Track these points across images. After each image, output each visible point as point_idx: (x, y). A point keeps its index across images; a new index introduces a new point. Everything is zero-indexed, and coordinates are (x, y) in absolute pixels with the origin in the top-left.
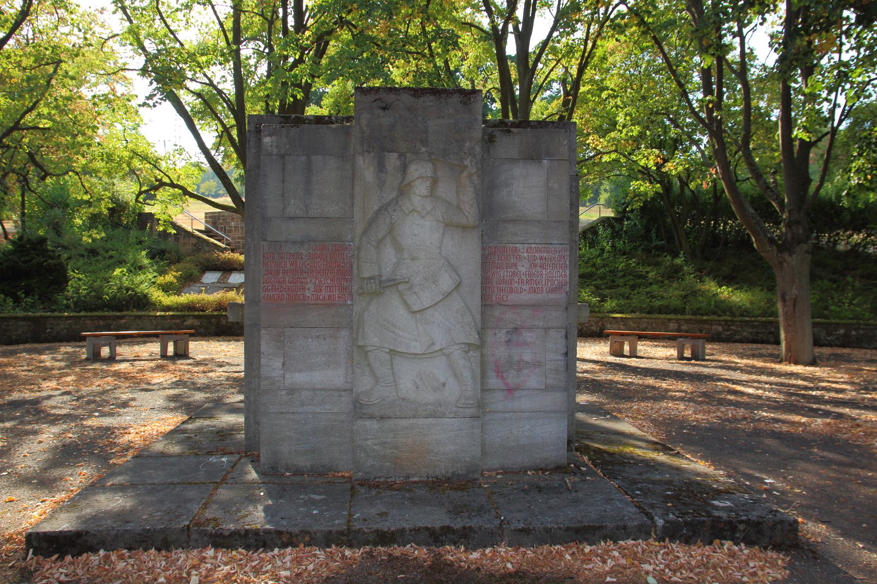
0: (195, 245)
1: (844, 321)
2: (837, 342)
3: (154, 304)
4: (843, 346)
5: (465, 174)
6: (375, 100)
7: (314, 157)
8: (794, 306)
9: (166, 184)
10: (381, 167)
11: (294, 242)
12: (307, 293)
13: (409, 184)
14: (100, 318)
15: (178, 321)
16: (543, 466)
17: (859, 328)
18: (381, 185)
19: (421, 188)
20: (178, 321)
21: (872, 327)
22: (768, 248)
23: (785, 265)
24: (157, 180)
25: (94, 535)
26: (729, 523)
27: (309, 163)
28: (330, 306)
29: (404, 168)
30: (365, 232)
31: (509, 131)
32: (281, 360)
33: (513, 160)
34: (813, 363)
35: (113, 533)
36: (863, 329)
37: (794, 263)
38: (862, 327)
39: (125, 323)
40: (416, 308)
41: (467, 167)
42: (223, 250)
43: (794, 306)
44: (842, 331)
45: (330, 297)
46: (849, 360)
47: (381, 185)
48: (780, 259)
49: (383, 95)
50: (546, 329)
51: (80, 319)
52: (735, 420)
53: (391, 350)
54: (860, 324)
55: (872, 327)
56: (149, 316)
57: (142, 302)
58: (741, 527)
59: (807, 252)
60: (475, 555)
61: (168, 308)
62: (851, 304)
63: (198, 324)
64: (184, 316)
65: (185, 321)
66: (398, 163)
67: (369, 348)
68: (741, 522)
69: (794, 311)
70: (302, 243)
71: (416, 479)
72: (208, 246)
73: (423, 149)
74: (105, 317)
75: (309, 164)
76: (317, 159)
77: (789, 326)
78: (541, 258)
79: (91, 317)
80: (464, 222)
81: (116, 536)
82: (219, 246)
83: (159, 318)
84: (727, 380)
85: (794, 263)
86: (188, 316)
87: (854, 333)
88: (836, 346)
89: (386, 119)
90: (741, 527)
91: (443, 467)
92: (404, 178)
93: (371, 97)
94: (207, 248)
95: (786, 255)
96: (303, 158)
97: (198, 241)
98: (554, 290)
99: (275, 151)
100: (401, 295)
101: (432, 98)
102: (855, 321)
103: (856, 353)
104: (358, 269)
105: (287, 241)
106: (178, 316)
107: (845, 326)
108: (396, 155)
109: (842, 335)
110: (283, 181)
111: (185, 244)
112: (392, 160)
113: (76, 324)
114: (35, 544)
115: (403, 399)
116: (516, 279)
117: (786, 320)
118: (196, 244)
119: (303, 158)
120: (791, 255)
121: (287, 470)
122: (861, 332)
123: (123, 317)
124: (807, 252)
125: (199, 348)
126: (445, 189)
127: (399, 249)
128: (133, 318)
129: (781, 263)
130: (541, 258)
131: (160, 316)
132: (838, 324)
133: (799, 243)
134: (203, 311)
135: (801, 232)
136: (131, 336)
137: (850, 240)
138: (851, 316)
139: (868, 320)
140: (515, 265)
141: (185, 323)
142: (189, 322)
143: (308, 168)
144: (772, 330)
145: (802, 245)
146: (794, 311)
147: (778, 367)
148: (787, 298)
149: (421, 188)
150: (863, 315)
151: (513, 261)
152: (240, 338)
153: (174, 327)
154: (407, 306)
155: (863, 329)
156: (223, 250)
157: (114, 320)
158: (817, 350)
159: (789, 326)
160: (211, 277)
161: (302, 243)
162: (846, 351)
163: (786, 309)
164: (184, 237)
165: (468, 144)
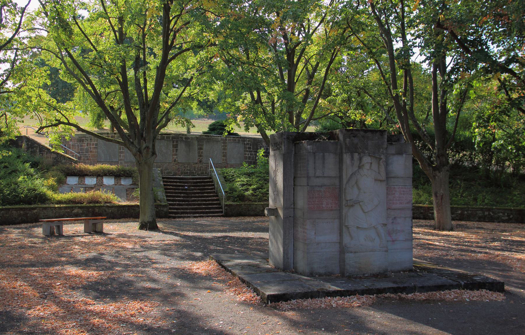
0: (55, 158)
1: (459, 206)
2: (457, 218)
3: (50, 200)
4: (461, 220)
5: (381, 161)
6: (351, 134)
7: (325, 154)
8: (442, 199)
9: (63, 123)
10: (352, 158)
11: (319, 186)
12: (324, 206)
13: (363, 165)
14: (21, 209)
15: (69, 210)
16: (405, 270)
17: (469, 210)
18: (353, 165)
19: (367, 166)
20: (69, 210)
21: (475, 209)
22: (428, 168)
23: (437, 177)
24: (56, 120)
25: (289, 295)
26: (483, 283)
27: (324, 156)
28: (332, 210)
29: (360, 159)
30: (347, 182)
31: (392, 144)
32: (314, 232)
33: (393, 154)
34: (452, 230)
35: (295, 294)
36: (471, 211)
37: (441, 176)
38: (470, 209)
39: (37, 212)
40: (366, 211)
41: (382, 158)
42: (76, 162)
43: (442, 199)
44: (460, 212)
45: (331, 207)
46: (468, 228)
47: (353, 165)
48: (434, 174)
49: (354, 132)
50: (405, 218)
51: (9, 210)
52: (442, 255)
53: (357, 227)
54: (469, 208)
55: (475, 209)
56: (51, 208)
57: (42, 198)
58: (487, 285)
59: (447, 171)
60: (410, 295)
61: (59, 202)
62: (462, 196)
63: (81, 212)
64: (72, 207)
65: (73, 210)
66: (358, 157)
67: (350, 226)
68: (487, 283)
69: (442, 202)
70: (321, 186)
71: (366, 275)
72: (65, 159)
73: (366, 152)
74: (24, 208)
75: (324, 156)
76: (326, 154)
77: (439, 210)
78: (403, 191)
79: (16, 208)
80: (381, 179)
81: (296, 295)
82: (73, 160)
83: (57, 209)
84: (424, 239)
85: (441, 176)
86: (75, 207)
87: (466, 212)
88: (457, 220)
89: (356, 141)
90: (487, 285)
91: (376, 270)
92: (360, 163)
93: (350, 133)
94: (63, 161)
95: (437, 172)
96: (322, 154)
97: (58, 156)
98: (408, 203)
99: (311, 151)
100: (361, 206)
101: (371, 133)
102: (466, 206)
103: (469, 223)
104: (345, 196)
105: (316, 186)
106: (69, 207)
107: (461, 209)
108: (357, 154)
109: (459, 214)
110: (315, 163)
111: (47, 157)
112: (356, 156)
113: (6, 214)
114: (270, 298)
115: (361, 245)
116: (395, 199)
117: (437, 207)
118: (56, 158)
119: (322, 154)
120: (439, 172)
121: (316, 274)
122: (470, 212)
123: (34, 209)
124: (447, 171)
125: (109, 227)
126: (375, 166)
127: (359, 189)
128: (42, 209)
129: (434, 176)
130: (403, 191)
131: (58, 207)
132: (457, 208)
133: (444, 166)
134: (81, 203)
135: (444, 160)
136: (68, 220)
137: (454, 158)
138: (463, 203)
139: (472, 205)
140: (394, 194)
141: (73, 212)
142: (76, 211)
143: (324, 158)
144: (422, 211)
145: (445, 167)
146: (442, 202)
147: (440, 232)
148: (438, 195)
149: (367, 166)
150: (469, 202)
151: (394, 192)
152: (137, 220)
153: (66, 214)
154: (362, 210)
155: (471, 211)
156: (76, 162)
157: (30, 210)
158: (454, 223)
159: (439, 210)
160: (72, 181)
161: (321, 186)
162: (463, 223)
163: (437, 201)
164: (47, 153)
165: (381, 150)
